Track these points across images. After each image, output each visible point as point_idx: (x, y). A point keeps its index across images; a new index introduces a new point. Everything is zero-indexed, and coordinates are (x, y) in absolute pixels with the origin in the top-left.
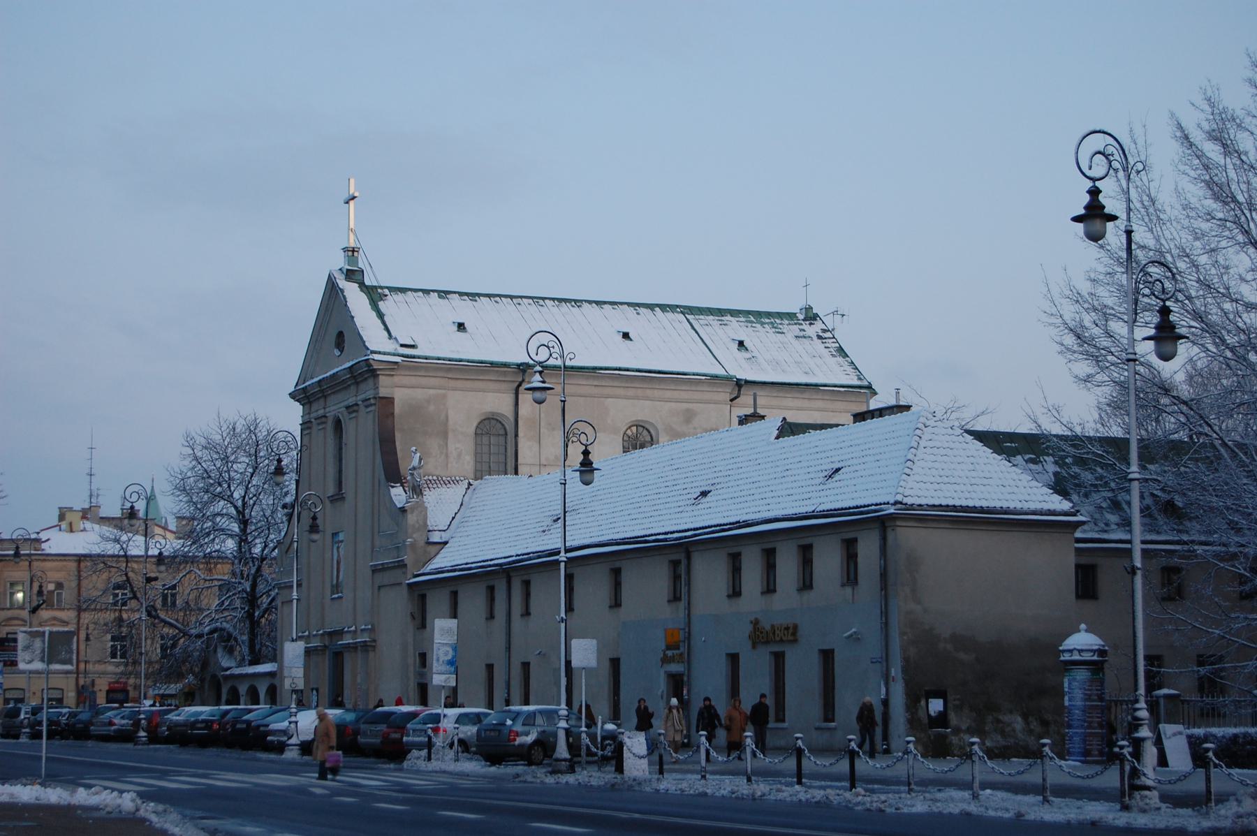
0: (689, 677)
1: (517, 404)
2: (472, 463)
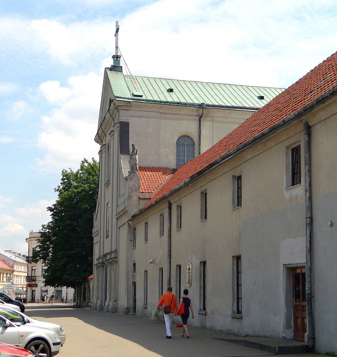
0: (311, 269)
1: (200, 128)
2: (175, 161)
